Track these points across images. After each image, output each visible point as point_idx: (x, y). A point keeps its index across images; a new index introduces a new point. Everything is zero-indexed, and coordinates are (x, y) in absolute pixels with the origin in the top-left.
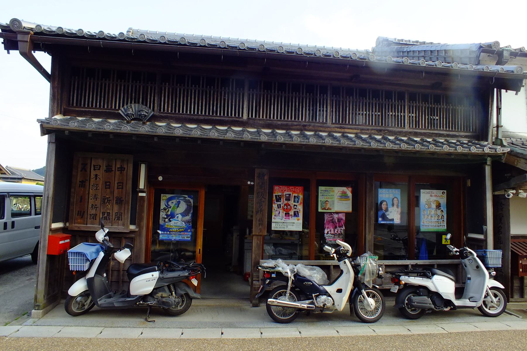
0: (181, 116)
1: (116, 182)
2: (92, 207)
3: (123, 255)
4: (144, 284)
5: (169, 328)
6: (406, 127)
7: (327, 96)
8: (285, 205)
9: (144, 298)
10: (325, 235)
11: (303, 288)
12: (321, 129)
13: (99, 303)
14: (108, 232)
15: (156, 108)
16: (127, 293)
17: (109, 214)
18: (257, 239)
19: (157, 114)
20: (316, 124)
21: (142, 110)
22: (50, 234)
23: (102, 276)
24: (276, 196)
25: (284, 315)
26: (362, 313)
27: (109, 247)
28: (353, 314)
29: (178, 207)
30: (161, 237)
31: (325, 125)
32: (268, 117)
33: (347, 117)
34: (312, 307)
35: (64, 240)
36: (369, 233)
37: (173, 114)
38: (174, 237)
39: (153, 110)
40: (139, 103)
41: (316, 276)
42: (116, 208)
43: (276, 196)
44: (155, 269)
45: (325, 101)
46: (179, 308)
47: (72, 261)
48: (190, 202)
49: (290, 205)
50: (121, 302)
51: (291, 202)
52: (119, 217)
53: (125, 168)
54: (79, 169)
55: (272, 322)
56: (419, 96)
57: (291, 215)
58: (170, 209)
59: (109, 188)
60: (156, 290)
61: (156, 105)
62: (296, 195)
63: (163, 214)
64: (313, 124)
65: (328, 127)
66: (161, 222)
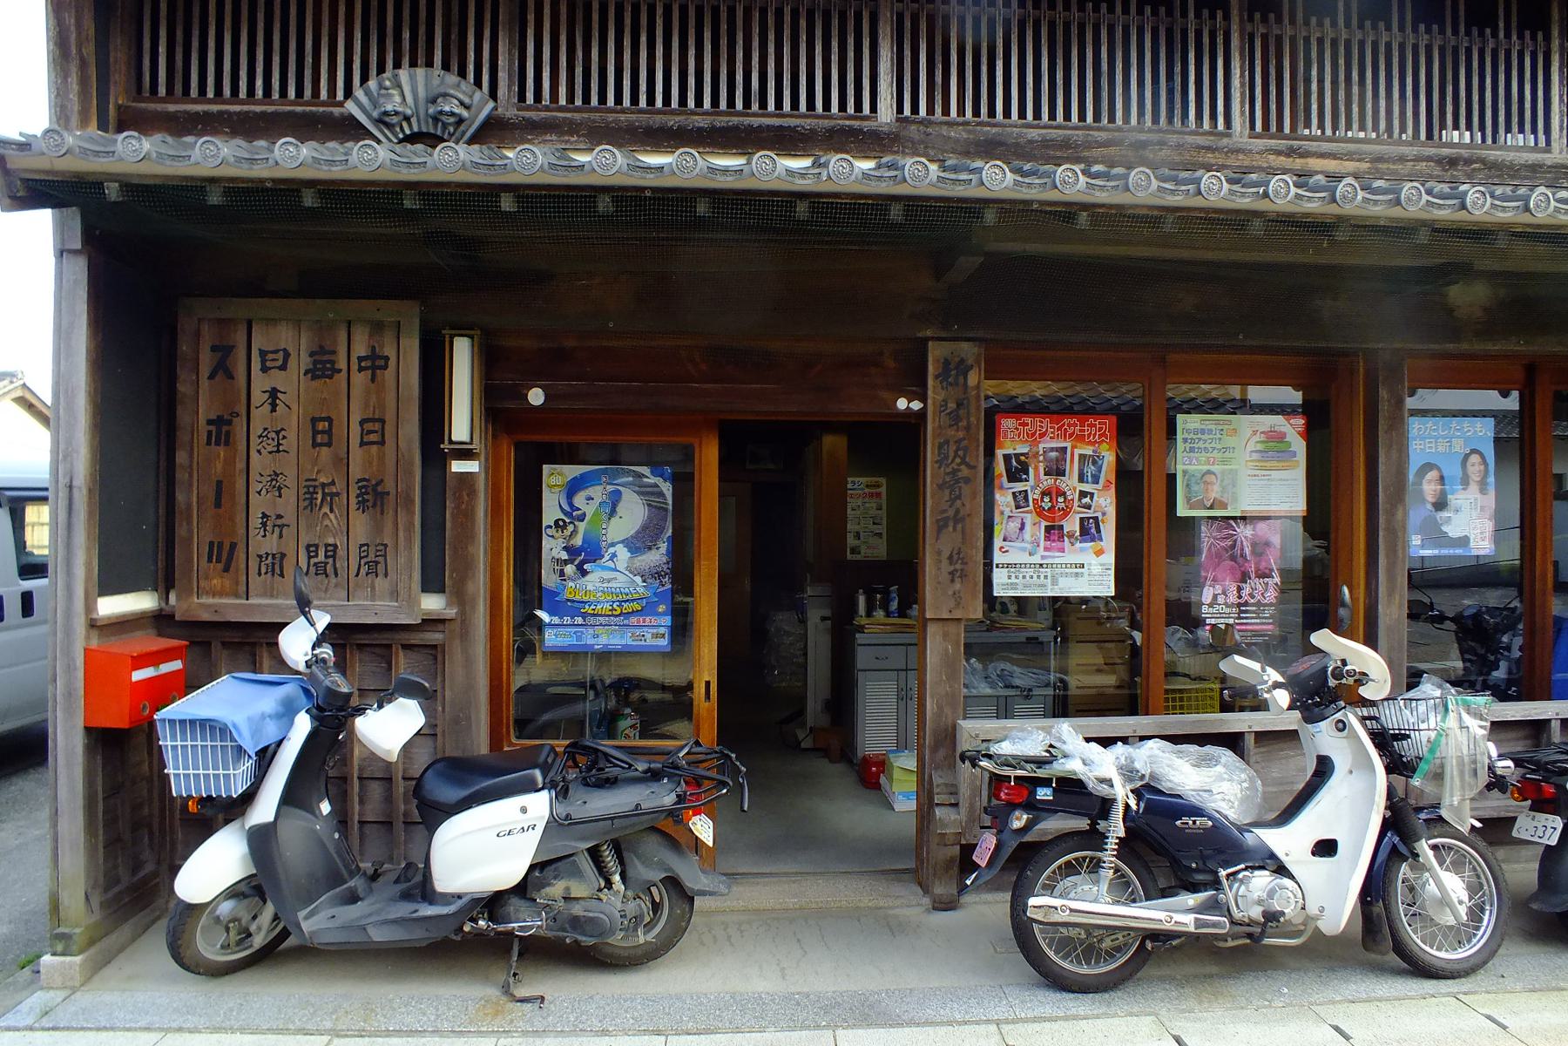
0: (611, 117)
1: (356, 418)
2: (264, 525)
3: (389, 728)
4: (485, 846)
5: (604, 1033)
6: (1555, 145)
7: (1227, 17)
8: (1043, 494)
9: (493, 903)
10: (1205, 609)
11: (1171, 845)
12: (1210, 158)
13: (306, 926)
14: (330, 626)
15: (502, 90)
16: (418, 878)
17: (332, 551)
18: (945, 635)
19: (509, 111)
20: (1190, 139)
21: (445, 95)
22: (94, 643)
23: (313, 810)
24: (1007, 458)
25: (1090, 952)
26: (1415, 938)
27: (331, 693)
28: (1380, 940)
29: (613, 513)
30: (551, 638)
31: (1225, 141)
32: (984, 110)
33: (1314, 107)
34: (1215, 925)
35: (156, 664)
36: (1390, 594)
37: (577, 110)
38: (604, 638)
39: (493, 94)
40: (429, 64)
41: (1215, 785)
42: (361, 526)
43: (1007, 458)
44: (533, 781)
45: (1220, 40)
46: (642, 940)
47: (175, 758)
48: (661, 494)
49: (1064, 494)
50: (395, 922)
51: (1071, 483)
52: (374, 563)
53: (387, 359)
54: (205, 371)
55: (1039, 986)
57: (1071, 535)
58: (582, 526)
59: (329, 445)
60: (541, 869)
61: (502, 76)
62: (1088, 451)
63: (552, 547)
64: (1173, 139)
65: (1238, 151)
66: (549, 579)
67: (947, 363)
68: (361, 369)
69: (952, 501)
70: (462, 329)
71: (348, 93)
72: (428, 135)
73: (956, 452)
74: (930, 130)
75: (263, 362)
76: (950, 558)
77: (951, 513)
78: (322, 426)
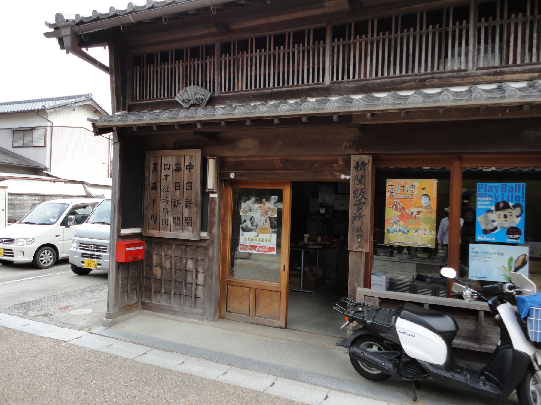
1: (185, 182)
35: (134, 247)
37: (253, 90)
45: (464, 33)
54: (151, 170)
56: (172, 52)
61: (216, 84)
67: (358, 162)
68: (187, 169)
69: (359, 210)
70: (212, 156)
71: (175, 95)
72: (196, 104)
73: (360, 193)
74: (341, 85)
75: (164, 167)
76: (357, 230)
77: (358, 214)
78: (178, 184)
